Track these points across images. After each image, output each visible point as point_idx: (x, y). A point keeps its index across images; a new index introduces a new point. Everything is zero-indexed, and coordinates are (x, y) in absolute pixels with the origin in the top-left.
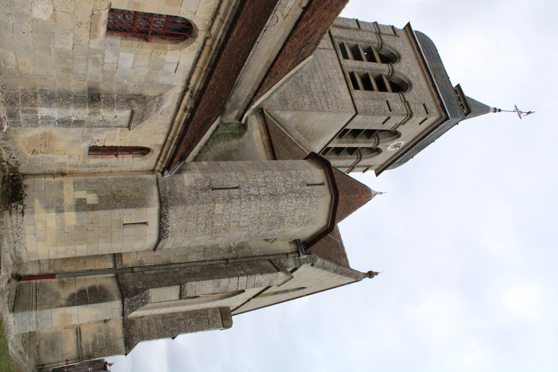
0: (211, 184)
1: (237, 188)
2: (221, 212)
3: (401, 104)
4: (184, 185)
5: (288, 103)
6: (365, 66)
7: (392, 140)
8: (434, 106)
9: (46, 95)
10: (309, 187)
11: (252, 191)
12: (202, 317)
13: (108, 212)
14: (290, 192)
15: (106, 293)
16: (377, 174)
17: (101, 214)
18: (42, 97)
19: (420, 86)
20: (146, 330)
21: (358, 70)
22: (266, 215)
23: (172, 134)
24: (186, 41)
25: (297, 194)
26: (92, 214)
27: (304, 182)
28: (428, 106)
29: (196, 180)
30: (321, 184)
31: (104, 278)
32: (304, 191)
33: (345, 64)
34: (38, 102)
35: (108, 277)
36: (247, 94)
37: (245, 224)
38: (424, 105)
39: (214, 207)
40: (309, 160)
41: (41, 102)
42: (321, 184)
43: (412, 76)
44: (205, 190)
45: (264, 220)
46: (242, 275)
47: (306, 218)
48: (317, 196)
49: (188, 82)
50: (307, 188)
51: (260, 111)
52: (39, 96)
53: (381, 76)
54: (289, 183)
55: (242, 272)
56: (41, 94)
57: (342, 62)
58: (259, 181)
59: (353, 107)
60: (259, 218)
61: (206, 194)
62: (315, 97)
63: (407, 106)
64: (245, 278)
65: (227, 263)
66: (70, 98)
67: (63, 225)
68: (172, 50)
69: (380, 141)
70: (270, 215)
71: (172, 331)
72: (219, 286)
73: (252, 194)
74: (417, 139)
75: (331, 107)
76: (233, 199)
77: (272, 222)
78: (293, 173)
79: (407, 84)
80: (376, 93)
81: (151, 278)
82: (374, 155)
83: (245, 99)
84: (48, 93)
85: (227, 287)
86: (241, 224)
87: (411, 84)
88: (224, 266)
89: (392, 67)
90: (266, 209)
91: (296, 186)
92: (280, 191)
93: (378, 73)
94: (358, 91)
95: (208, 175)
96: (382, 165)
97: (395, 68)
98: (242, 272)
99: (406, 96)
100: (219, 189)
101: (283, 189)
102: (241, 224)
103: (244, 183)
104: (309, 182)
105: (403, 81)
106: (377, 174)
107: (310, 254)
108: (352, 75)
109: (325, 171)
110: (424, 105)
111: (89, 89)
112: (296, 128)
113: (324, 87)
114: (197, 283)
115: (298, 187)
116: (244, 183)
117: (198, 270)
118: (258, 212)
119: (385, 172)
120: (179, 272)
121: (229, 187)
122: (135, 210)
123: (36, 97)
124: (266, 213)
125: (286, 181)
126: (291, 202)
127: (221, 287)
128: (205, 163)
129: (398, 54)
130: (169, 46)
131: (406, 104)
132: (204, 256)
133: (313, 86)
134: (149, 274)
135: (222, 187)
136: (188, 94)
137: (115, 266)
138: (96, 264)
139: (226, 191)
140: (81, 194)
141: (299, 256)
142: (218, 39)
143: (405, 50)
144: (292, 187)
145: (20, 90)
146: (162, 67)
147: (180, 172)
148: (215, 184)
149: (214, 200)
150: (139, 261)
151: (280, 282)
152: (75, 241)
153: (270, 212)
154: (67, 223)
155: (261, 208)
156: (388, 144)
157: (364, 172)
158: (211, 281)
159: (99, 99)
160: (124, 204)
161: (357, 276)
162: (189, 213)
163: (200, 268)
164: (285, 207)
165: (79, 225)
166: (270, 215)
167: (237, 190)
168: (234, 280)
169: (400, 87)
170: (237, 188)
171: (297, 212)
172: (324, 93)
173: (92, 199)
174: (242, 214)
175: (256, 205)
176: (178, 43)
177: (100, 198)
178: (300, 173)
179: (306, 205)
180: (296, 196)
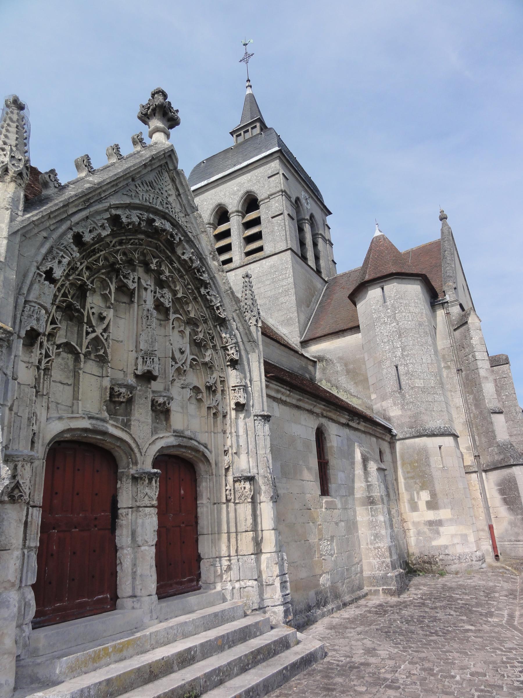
0: (397, 391)
1: (397, 367)
2: (422, 381)
3: (273, 202)
4: (401, 416)
5: (291, 318)
6: (236, 240)
7: (301, 205)
8: (268, 166)
9: (375, 540)
10: (388, 299)
11: (399, 354)
12: (499, 385)
13: (436, 483)
14: (395, 318)
15: (506, 479)
16: (330, 213)
17: (438, 487)
18: (377, 543)
19: (248, 182)
20: (517, 437)
21: (242, 248)
22: (419, 340)
23: (371, 431)
24: (324, 431)
25: (396, 312)
26: (440, 495)
27: (383, 306)
28: (270, 173)
29: (395, 404)
30: (383, 289)
31: (487, 481)
32: (392, 305)
33: (239, 262)
34: (382, 546)
35: (487, 478)
36: (296, 360)
37: (429, 358)
38: (269, 177)
39: (419, 387)
40: (356, 300)
41: (382, 543)
42: (383, 289)
43: (238, 190)
44: (403, 396)
45: (423, 340)
46: (474, 356)
47: (416, 301)
48: (396, 293)
49: (343, 425)
50: (388, 303)
51: (305, 343)
52: (377, 545)
53: (244, 224)
54: (386, 319)
55: (470, 356)
56: (375, 544)
57: (238, 265)
58: (387, 347)
59: (284, 253)
60: (422, 345)
61: (407, 396)
62: (280, 291)
63: (273, 196)
64: (477, 354)
65: (461, 370)
66: (374, 520)
67: (451, 520)
68: (331, 442)
69: (303, 217)
70: (418, 336)
71: (516, 413)
72: (487, 377)
73: (402, 354)
74: (299, 178)
75: (287, 275)
76: (408, 371)
77: (424, 332)
78: (375, 316)
79: (247, 196)
80: (263, 228)
81: (484, 440)
82: (315, 221)
83: (300, 361)
84: (373, 538)
85: (487, 369)
86: (429, 361)
87: (247, 192)
88: (464, 373)
89: (233, 213)
90: (414, 340)
91: (388, 313)
92: (395, 328)
93: (241, 227)
94: (265, 248)
95: (388, 394)
96: (322, 210)
97: (234, 209)
98: (470, 356)
99: (263, 197)
100: (400, 383)
101: (393, 325)
102: (429, 361)
103: (392, 362)
104: (381, 301)
105: (245, 200)
106: (330, 213)
107: (444, 292)
108: (248, 254)
109: (370, 286)
110: (269, 177)
111: (364, 506)
112: (308, 307)
113: (268, 282)
114: (486, 397)
115: (389, 311)
116: (392, 362)
117: (471, 397)
118: (417, 347)
119: (326, 204)
120: (474, 414)
121: (397, 375)
122: (431, 458)
123: (379, 547)
124: (417, 339)
125: (385, 323)
126: (405, 316)
127: (487, 375)
128: (373, 396)
129: (217, 206)
130: (328, 445)
131: (271, 197)
132: (456, 391)
133: (269, 294)
134: (480, 441)
135: (398, 381)
136: (351, 423)
137: (475, 472)
138: (474, 489)
139: (402, 378)
140: (422, 505)
141: (447, 302)
142: (323, 407)
143: (211, 199)
144: (389, 317)
145: (374, 561)
146: (340, 448)
147: (389, 419)
148: (396, 388)
149: (412, 388)
150: (467, 450)
151: (477, 321)
152: (463, 509)
153: (416, 336)
154: (450, 516)
155: (413, 345)
156: (305, 208)
157: (329, 228)
158: (483, 385)
159: (371, 497)
160: (427, 468)
161: (448, 235)
162: (426, 410)
163: (468, 395)
164: (409, 323)
165: (450, 507)
166: (418, 336)
167: (399, 368)
168: (480, 364)
169: (251, 203)
170: (397, 367)
171: (412, 310)
172: (273, 282)
173: (425, 496)
174: (421, 362)
175: (412, 349)
176: (325, 438)
177: (422, 488)
178: (375, 310)
179: (405, 302)
180: (398, 313)
